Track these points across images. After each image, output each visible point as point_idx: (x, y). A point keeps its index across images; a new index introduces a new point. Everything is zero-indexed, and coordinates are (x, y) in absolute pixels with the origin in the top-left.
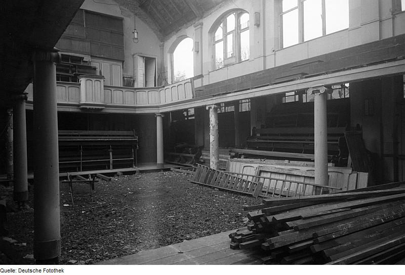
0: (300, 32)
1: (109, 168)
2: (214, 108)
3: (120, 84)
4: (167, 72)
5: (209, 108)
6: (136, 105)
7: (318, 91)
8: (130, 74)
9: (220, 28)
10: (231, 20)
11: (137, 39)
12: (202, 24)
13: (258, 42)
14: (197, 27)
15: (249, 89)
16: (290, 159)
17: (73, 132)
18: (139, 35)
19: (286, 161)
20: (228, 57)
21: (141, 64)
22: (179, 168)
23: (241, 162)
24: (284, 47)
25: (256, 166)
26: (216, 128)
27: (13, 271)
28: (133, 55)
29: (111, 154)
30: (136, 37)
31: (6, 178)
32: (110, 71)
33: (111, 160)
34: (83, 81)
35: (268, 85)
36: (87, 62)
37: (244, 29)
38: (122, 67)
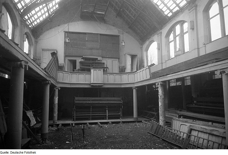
0: (222, 29)
1: (106, 119)
2: (161, 84)
3: (117, 71)
4: (144, 62)
5: (158, 84)
6: (122, 83)
7: (224, 72)
8: (123, 65)
9: (172, 33)
10: (178, 28)
11: (124, 46)
12: (161, 33)
13: (194, 40)
14: (158, 35)
15: (179, 72)
16: (213, 122)
17: (88, 98)
18: (128, 43)
19: (210, 123)
20: (177, 51)
21: (129, 59)
22: (146, 121)
23: (179, 121)
24: (212, 41)
25: (188, 125)
26: (163, 97)
27: (7, 153)
28: (125, 54)
29: (107, 111)
30: (123, 45)
31: (52, 122)
32: (111, 64)
33: (107, 114)
34: (92, 71)
35: (191, 69)
36: (100, 60)
37: (186, 32)
38: (118, 61)
